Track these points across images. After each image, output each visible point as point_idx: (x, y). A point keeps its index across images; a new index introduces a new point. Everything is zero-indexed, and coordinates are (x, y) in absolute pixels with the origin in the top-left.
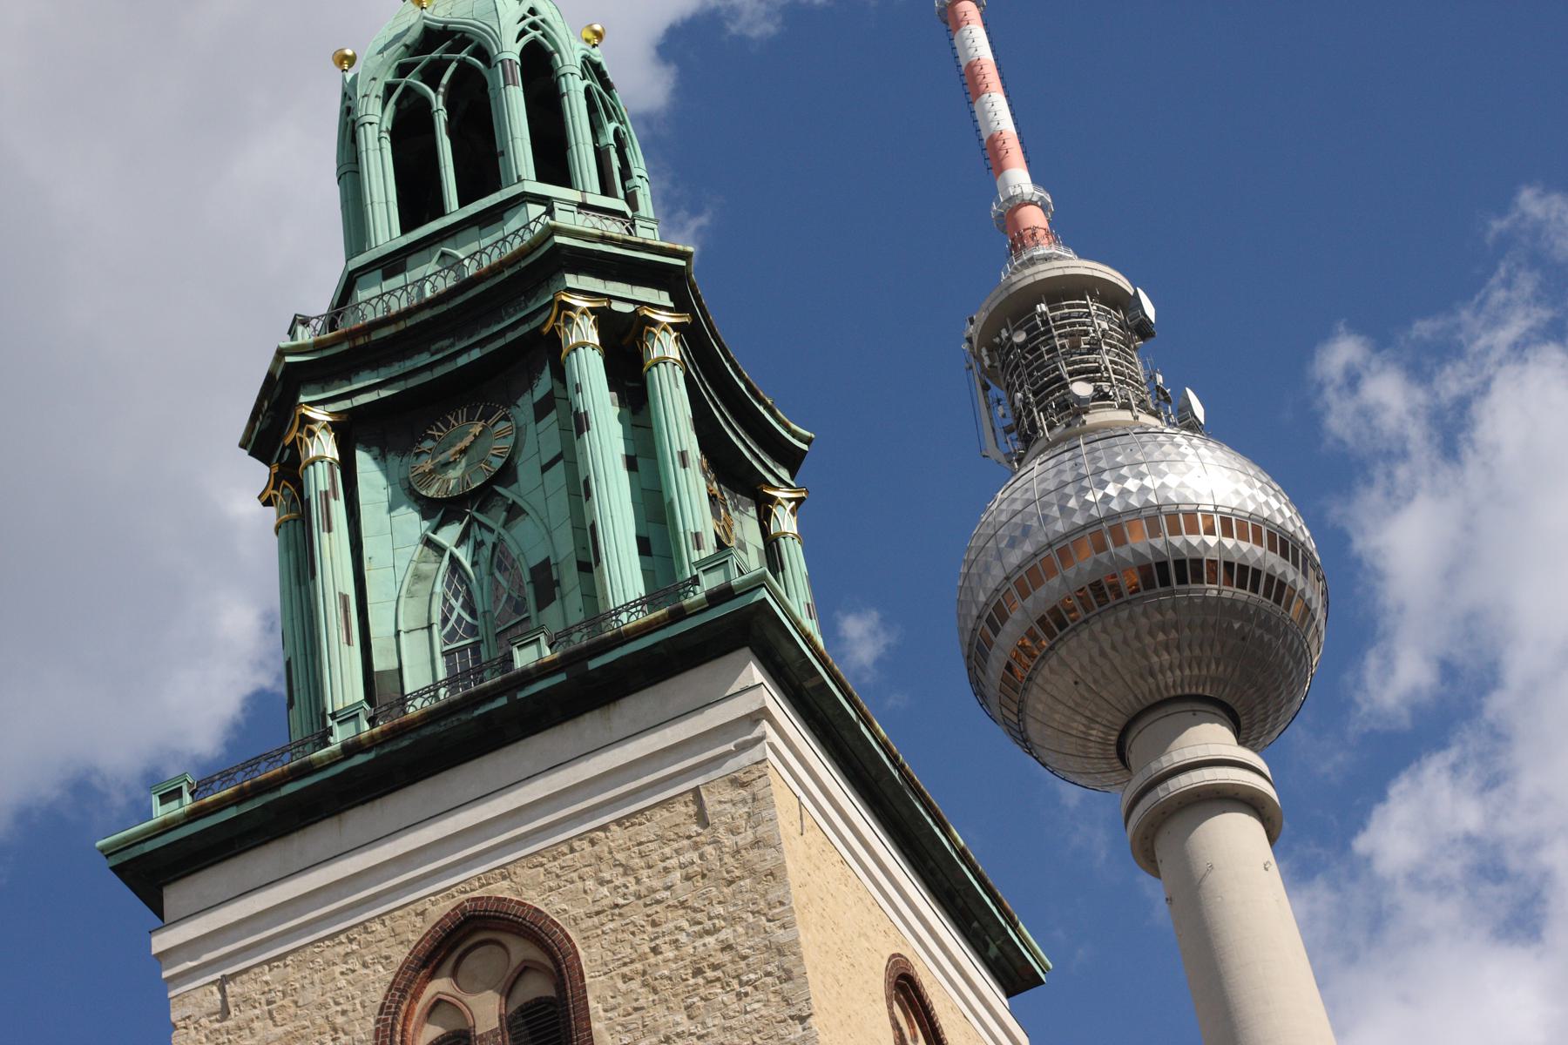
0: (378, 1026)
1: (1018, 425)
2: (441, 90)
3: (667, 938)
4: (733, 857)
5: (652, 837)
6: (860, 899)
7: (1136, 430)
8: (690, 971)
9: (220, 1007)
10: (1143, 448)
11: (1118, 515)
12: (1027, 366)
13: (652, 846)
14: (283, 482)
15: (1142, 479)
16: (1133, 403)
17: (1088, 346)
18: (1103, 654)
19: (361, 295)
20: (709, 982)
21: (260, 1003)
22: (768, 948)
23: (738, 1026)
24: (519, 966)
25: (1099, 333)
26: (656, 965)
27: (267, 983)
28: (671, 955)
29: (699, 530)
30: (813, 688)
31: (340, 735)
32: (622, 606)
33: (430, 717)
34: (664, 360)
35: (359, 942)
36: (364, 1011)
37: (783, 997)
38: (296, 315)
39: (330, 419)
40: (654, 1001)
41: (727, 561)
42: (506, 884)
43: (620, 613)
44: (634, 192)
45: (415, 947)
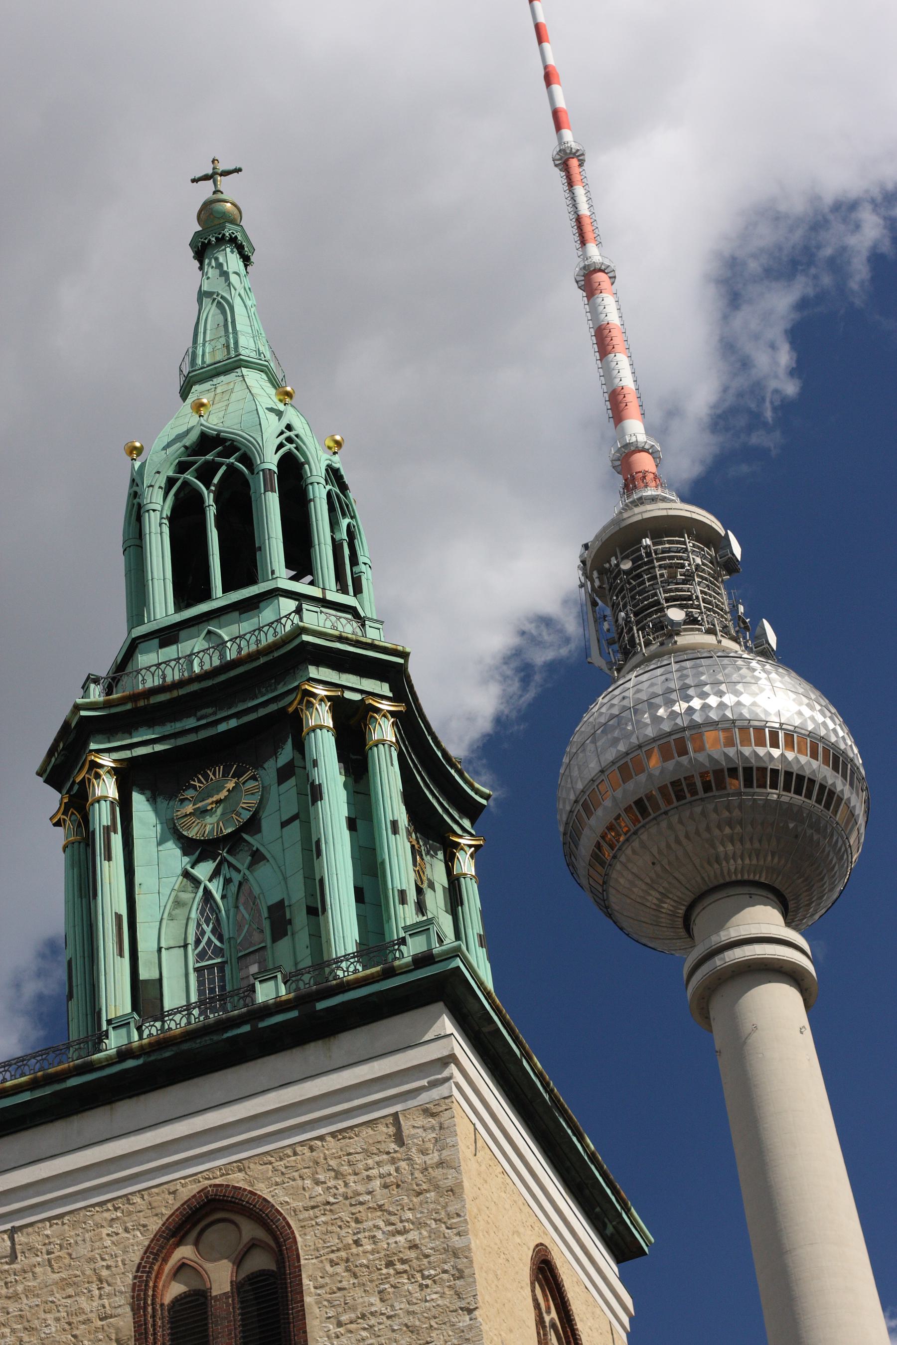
0: (135, 1281)
1: (619, 639)
2: (213, 488)
3: (367, 1234)
4: (422, 1173)
5: (359, 1150)
6: (515, 1202)
7: (719, 654)
8: (383, 1263)
9: (9, 1252)
10: (724, 670)
11: (699, 726)
12: (631, 590)
13: (358, 1157)
14: (72, 809)
15: (721, 697)
16: (718, 628)
17: (683, 577)
18: (678, 842)
19: (144, 659)
20: (398, 1273)
21: (41, 1253)
22: (446, 1250)
23: (419, 1312)
24: (248, 1243)
25: (693, 567)
26: (357, 1255)
27: (48, 1236)
28: (369, 1248)
29: (404, 888)
30: (489, 1032)
31: (114, 1042)
32: (344, 956)
33: (189, 1035)
34: (382, 742)
35: (123, 1211)
36: (124, 1268)
37: (456, 1291)
38: (89, 674)
39: (112, 765)
40: (354, 1284)
41: (429, 929)
42: (241, 1175)
43: (342, 961)
44: (360, 577)
45: (167, 1220)
